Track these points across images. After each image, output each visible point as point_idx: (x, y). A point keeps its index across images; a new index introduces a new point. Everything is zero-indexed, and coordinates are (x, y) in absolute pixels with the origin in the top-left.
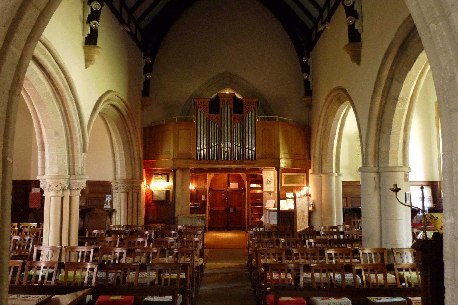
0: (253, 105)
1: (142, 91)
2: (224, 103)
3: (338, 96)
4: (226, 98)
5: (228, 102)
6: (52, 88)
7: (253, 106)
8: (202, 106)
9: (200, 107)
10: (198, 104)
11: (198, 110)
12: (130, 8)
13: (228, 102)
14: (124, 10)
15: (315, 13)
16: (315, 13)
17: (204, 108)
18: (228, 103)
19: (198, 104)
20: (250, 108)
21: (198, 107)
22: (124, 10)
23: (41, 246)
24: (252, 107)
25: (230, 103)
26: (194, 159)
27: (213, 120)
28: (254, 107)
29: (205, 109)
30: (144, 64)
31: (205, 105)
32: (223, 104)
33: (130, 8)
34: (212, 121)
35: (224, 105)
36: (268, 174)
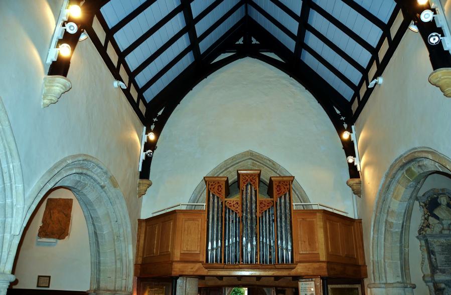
0: (286, 185)
1: (140, 172)
2: (246, 183)
3: (407, 168)
4: (249, 176)
5: (251, 181)
6: (173, 239)
7: (286, 187)
8: (216, 188)
9: (214, 188)
10: (211, 184)
11: (211, 193)
12: (140, 87)
13: (251, 181)
14: (141, 102)
15: (373, 34)
16: (355, 76)
17: (218, 189)
18: (251, 183)
19: (211, 184)
20: (283, 190)
21: (211, 188)
22: (141, 102)
23: (325, 273)
24: (285, 188)
25: (254, 183)
26: (202, 262)
27: (231, 206)
28: (288, 188)
29: (221, 191)
30: (146, 141)
31: (220, 186)
32: (245, 185)
33: (140, 87)
34: (230, 207)
35: (247, 186)
36: (307, 286)
